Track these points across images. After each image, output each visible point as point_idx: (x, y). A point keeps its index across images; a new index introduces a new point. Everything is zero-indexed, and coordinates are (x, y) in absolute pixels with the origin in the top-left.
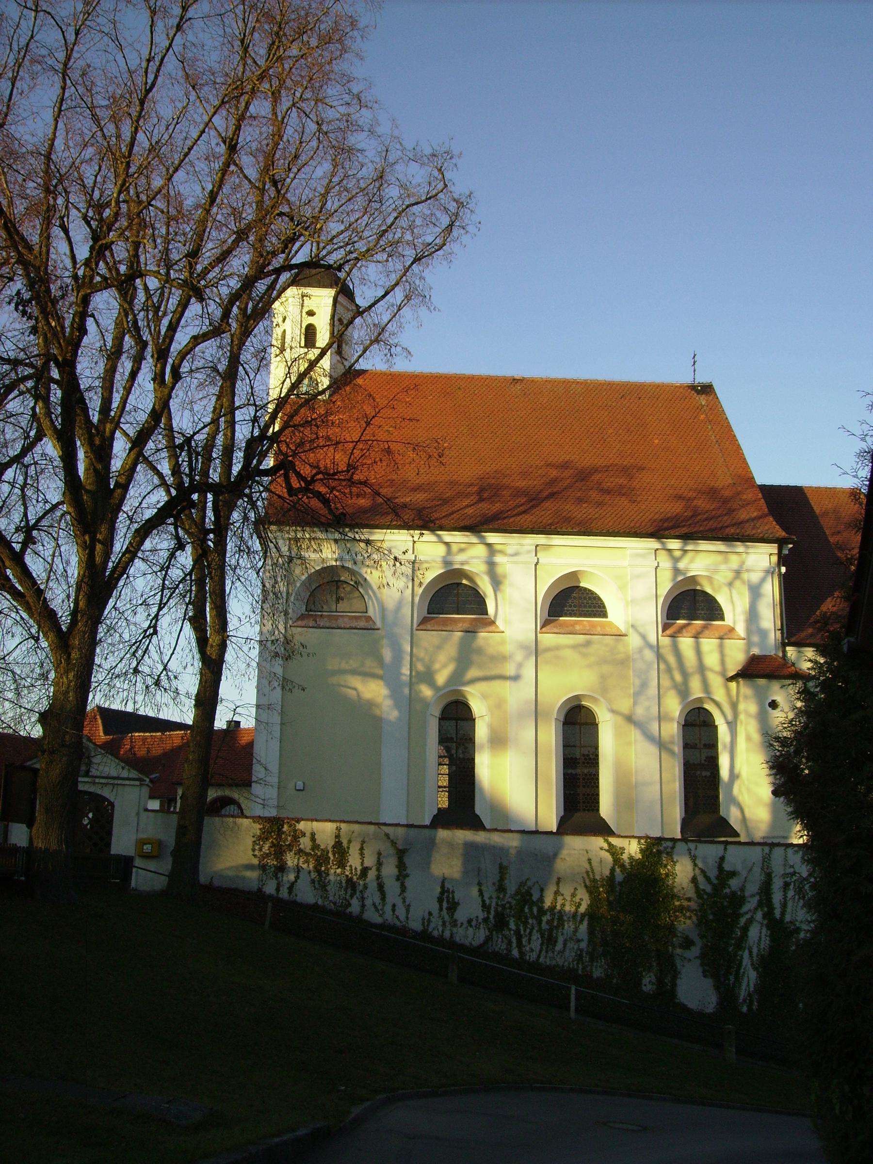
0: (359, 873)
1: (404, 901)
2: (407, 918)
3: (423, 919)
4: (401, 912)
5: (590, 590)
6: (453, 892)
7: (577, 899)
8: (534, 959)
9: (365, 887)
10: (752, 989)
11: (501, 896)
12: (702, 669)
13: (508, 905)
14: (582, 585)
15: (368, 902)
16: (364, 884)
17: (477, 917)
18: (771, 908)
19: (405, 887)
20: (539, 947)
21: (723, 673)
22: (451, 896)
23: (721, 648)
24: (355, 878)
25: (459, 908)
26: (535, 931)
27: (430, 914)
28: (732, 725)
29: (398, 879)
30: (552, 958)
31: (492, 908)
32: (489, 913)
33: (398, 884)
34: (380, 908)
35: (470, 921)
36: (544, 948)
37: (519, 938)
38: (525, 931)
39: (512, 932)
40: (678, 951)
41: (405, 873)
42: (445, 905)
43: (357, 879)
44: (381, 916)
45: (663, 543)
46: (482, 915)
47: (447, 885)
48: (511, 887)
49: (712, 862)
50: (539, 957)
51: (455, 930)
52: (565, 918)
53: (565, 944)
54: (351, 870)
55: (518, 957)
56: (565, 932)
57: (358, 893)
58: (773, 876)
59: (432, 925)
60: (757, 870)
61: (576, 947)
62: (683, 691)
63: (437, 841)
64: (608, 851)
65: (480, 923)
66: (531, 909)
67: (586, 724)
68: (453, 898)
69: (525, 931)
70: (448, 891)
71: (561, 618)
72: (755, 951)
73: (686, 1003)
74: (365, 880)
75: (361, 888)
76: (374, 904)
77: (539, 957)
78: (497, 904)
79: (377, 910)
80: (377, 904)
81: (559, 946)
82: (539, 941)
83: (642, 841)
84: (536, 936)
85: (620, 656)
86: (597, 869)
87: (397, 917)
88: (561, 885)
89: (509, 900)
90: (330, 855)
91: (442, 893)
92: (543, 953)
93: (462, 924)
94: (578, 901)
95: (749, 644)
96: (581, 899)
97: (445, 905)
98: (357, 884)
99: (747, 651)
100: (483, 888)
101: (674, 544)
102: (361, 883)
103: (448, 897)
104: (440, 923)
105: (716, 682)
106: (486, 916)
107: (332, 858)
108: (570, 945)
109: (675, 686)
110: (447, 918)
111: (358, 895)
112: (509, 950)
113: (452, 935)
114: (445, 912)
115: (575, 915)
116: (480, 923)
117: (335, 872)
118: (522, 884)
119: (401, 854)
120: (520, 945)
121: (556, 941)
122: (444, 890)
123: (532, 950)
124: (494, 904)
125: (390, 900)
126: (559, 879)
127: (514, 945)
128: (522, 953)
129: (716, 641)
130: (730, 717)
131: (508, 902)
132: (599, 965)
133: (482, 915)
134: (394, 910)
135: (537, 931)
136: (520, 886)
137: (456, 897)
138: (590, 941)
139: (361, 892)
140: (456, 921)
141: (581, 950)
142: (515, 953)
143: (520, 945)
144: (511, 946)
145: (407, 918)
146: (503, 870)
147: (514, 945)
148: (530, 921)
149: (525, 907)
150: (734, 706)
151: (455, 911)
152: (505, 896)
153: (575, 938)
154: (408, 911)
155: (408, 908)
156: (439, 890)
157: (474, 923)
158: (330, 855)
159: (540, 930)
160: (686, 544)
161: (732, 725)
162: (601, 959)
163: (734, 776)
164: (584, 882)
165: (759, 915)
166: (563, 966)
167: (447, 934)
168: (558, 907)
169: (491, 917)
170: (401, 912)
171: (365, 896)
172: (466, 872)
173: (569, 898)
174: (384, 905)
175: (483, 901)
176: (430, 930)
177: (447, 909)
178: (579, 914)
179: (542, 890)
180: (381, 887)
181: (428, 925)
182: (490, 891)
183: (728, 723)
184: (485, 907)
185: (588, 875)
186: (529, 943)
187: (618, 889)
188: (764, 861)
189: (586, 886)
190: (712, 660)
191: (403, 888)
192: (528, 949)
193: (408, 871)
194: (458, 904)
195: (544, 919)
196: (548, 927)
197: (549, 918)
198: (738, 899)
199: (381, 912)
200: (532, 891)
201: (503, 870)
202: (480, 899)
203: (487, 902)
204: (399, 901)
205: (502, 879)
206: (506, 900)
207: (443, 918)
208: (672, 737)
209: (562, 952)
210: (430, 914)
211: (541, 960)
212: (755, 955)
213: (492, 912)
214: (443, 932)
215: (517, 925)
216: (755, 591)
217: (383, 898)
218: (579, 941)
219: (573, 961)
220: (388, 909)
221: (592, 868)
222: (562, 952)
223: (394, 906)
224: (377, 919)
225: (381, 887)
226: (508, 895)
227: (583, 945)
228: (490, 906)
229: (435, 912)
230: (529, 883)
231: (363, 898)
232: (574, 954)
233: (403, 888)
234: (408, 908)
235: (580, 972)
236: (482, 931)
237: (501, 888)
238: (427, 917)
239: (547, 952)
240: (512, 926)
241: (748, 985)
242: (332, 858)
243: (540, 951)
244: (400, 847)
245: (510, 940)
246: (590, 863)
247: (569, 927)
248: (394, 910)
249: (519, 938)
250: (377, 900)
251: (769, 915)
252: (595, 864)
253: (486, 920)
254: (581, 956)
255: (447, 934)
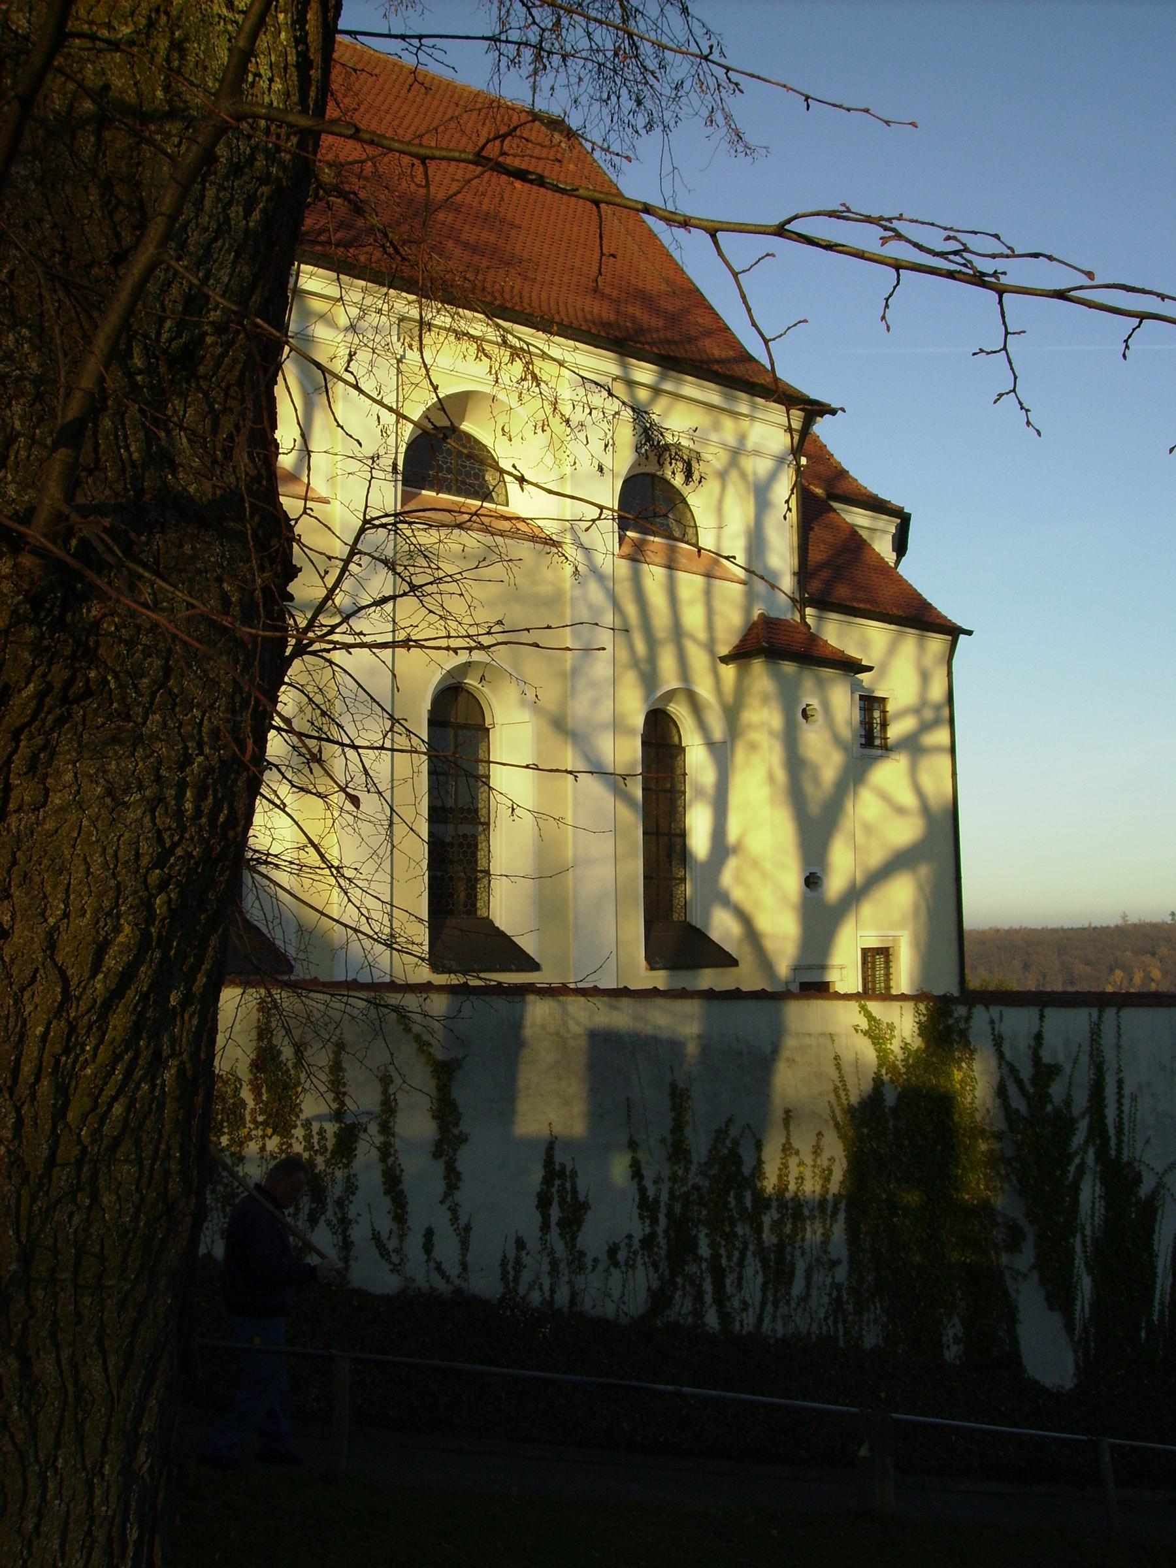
0: (331, 1143)
1: (455, 1219)
2: (464, 1266)
3: (504, 1263)
4: (447, 1249)
5: (477, 441)
6: (574, 1174)
7: (823, 1161)
8: (751, 1328)
9: (351, 1187)
10: (1087, 1315)
11: (680, 1173)
12: (678, 632)
13: (695, 1196)
14: (467, 426)
15: (359, 1233)
16: (348, 1178)
17: (630, 1237)
18: (1105, 1139)
19: (459, 1174)
20: (758, 1297)
21: (710, 646)
22: (568, 1185)
23: (708, 593)
24: (320, 1160)
25: (590, 1217)
26: (749, 1253)
27: (520, 1244)
28: (722, 754)
29: (437, 1154)
30: (788, 1318)
31: (662, 1204)
32: (654, 1221)
33: (439, 1167)
34: (392, 1245)
35: (612, 1252)
36: (771, 1298)
37: (718, 1274)
38: (729, 1258)
39: (704, 1265)
40: (1004, 1259)
41: (456, 1132)
42: (555, 1213)
43: (327, 1162)
44: (396, 1269)
45: (624, 366)
46: (639, 1230)
47: (559, 1157)
48: (699, 1146)
49: (1023, 1044)
50: (760, 1320)
51: (580, 1279)
52: (806, 1212)
53: (808, 1278)
54: (308, 1137)
55: (717, 1327)
56: (806, 1245)
57: (331, 1208)
58: (1105, 1068)
59: (526, 1276)
60: (1084, 1059)
61: (829, 1280)
62: (649, 677)
63: (528, 1032)
64: (865, 1033)
65: (635, 1253)
66: (740, 1199)
67: (465, 726)
68: (574, 1191)
69: (729, 1258)
70: (562, 1173)
71: (424, 492)
72: (1088, 1232)
73: (1037, 1377)
74: (347, 1166)
75: (337, 1191)
76: (376, 1237)
77: (760, 1320)
78: (672, 1197)
79: (384, 1253)
80: (384, 1235)
81: (798, 1287)
82: (760, 1279)
83: (922, 1007)
84: (752, 1266)
85: (545, 589)
86: (851, 1081)
87: (439, 1268)
88: (792, 1128)
89: (697, 1180)
90: (246, 1094)
91: (547, 1181)
92: (769, 1306)
93: (596, 1260)
94: (825, 1164)
95: (751, 597)
96: (832, 1159)
97: (555, 1213)
98: (327, 1179)
99: (748, 610)
100: (642, 1156)
101: (644, 373)
102: (339, 1174)
103: (562, 1190)
104: (546, 1267)
105: (699, 660)
106: (648, 1230)
107: (251, 1104)
108: (818, 1277)
109: (635, 663)
110: (560, 1248)
111: (329, 1214)
112: (698, 1314)
113: (573, 1296)
114: (555, 1230)
115: (822, 1202)
116: (635, 1253)
117: (263, 1149)
118: (720, 1135)
119: (445, 1072)
120: (721, 1298)
121: (792, 1274)
122: (553, 1173)
123: (745, 1306)
124: (664, 1197)
125: (417, 1221)
126: (788, 1112)
127: (708, 1298)
128: (724, 1317)
129: (699, 580)
130: (718, 731)
131: (696, 1187)
132: (872, 1316)
133: (639, 1230)
134: (428, 1248)
135: (754, 1255)
136: (716, 1140)
137: (579, 1189)
138: (851, 1261)
139: (340, 1203)
140: (582, 1254)
141: (838, 1287)
142: (711, 1319)
143: (721, 1298)
144: (703, 1303)
145: (464, 1266)
146: (678, 1098)
147: (708, 1298)
148: (739, 1230)
149: (728, 1195)
150: (732, 713)
151: (580, 1227)
152: (687, 1170)
153: (825, 1259)
154: (465, 1244)
155: (464, 1235)
156: (536, 1175)
157: (622, 1256)
158: (246, 1094)
159: (761, 1251)
160: (663, 377)
161: (722, 754)
162: (874, 1303)
163: (721, 848)
164: (834, 1118)
165: (1090, 1157)
166: (809, 1334)
167: (563, 1296)
168: (792, 1187)
169: (660, 1230)
170: (447, 1249)
171: (351, 1215)
172: (597, 1115)
173: (808, 1160)
174: (402, 1237)
175: (642, 1191)
176: (522, 1290)
177: (562, 1224)
178: (829, 1197)
179: (759, 1146)
180: (392, 1181)
181: (516, 1279)
182: (656, 1165)
183: (710, 744)
184: (647, 1207)
185: (838, 1097)
186: (740, 1287)
187: (890, 1125)
188: (1092, 1040)
189: (837, 1125)
190: (693, 617)
191: (453, 1178)
192: (736, 1304)
193: (465, 1127)
194: (584, 1206)
195: (767, 1220)
196: (775, 1240)
197: (776, 1216)
198: (1064, 1124)
199: (395, 1259)
200: (741, 1151)
201: (678, 1098)
202: (634, 1186)
203: (651, 1193)
204: (441, 1219)
205: (678, 1127)
206: (691, 1183)
207: (552, 1252)
208: (633, 765)
209: (805, 1298)
210: (520, 1244)
211: (766, 1326)
212: (1088, 1239)
213: (663, 1220)
214: (552, 1291)
215: (713, 1245)
216: (761, 494)
217: (400, 1215)
218: (834, 1264)
219: (826, 1319)
220: (414, 1244)
221: (841, 1077)
222: (805, 1298)
223: (429, 1233)
224: (384, 1282)
225: (392, 1181)
226: (694, 1168)
227: (841, 1273)
228: (657, 1201)
229: (533, 1242)
230: (734, 1131)
231: (345, 1223)
232: (826, 1300)
233: (453, 1178)
234: (464, 1235)
235: (841, 1344)
236: (641, 1273)
237: (678, 1152)
238: (512, 1254)
239: (775, 1304)
240: (704, 1251)
241: (1082, 1310)
242: (251, 1104)
243: (763, 1304)
244: (440, 1055)
245: (700, 1286)
246: (838, 1067)
247: (813, 1233)
248: (428, 1248)
249: (718, 1274)
250: (386, 1225)
251: (1102, 1154)
252: (847, 1069)
253: (648, 1242)
254: (838, 1300)
255: (563, 1296)
